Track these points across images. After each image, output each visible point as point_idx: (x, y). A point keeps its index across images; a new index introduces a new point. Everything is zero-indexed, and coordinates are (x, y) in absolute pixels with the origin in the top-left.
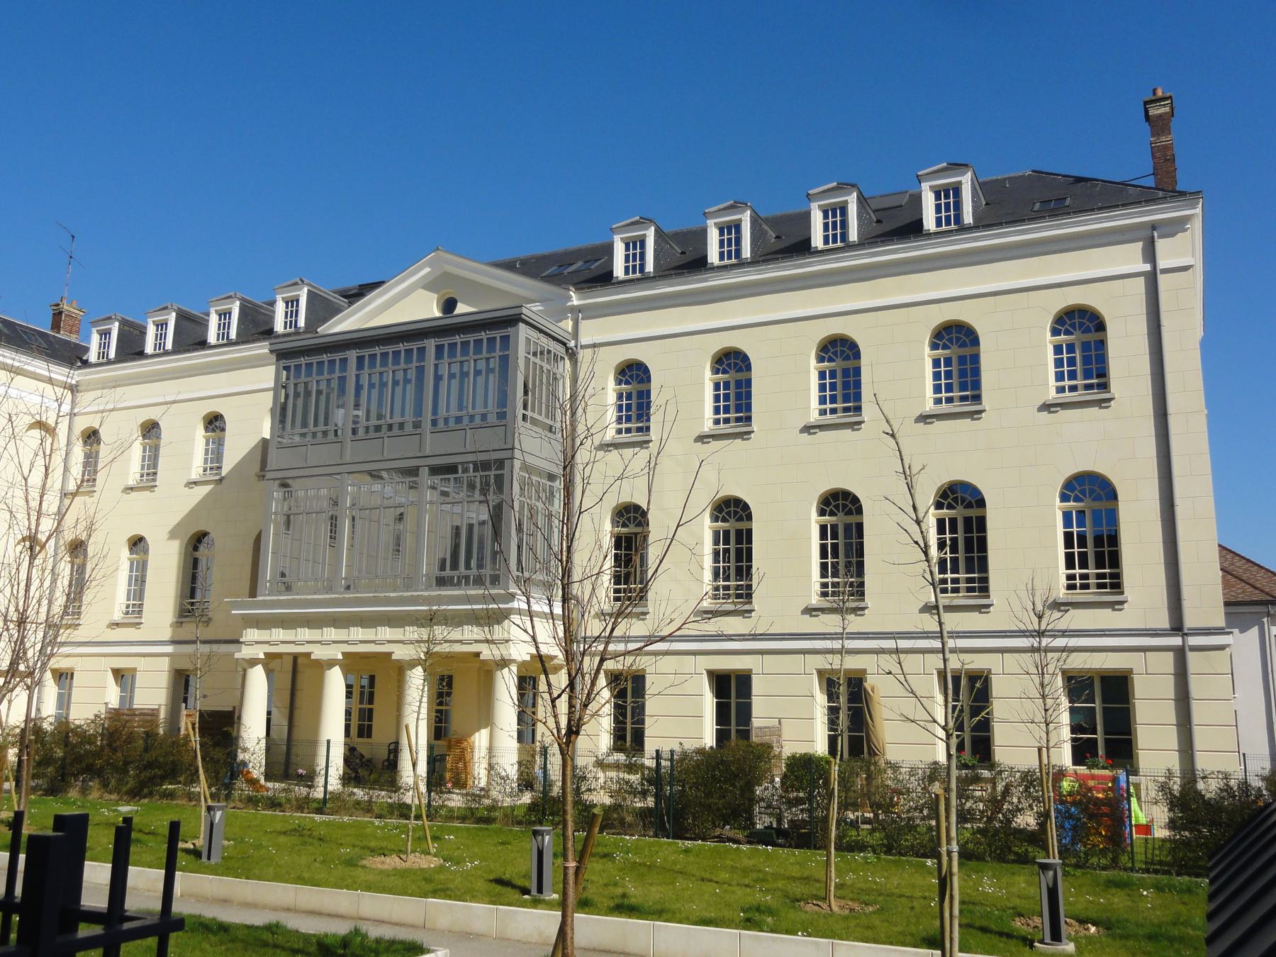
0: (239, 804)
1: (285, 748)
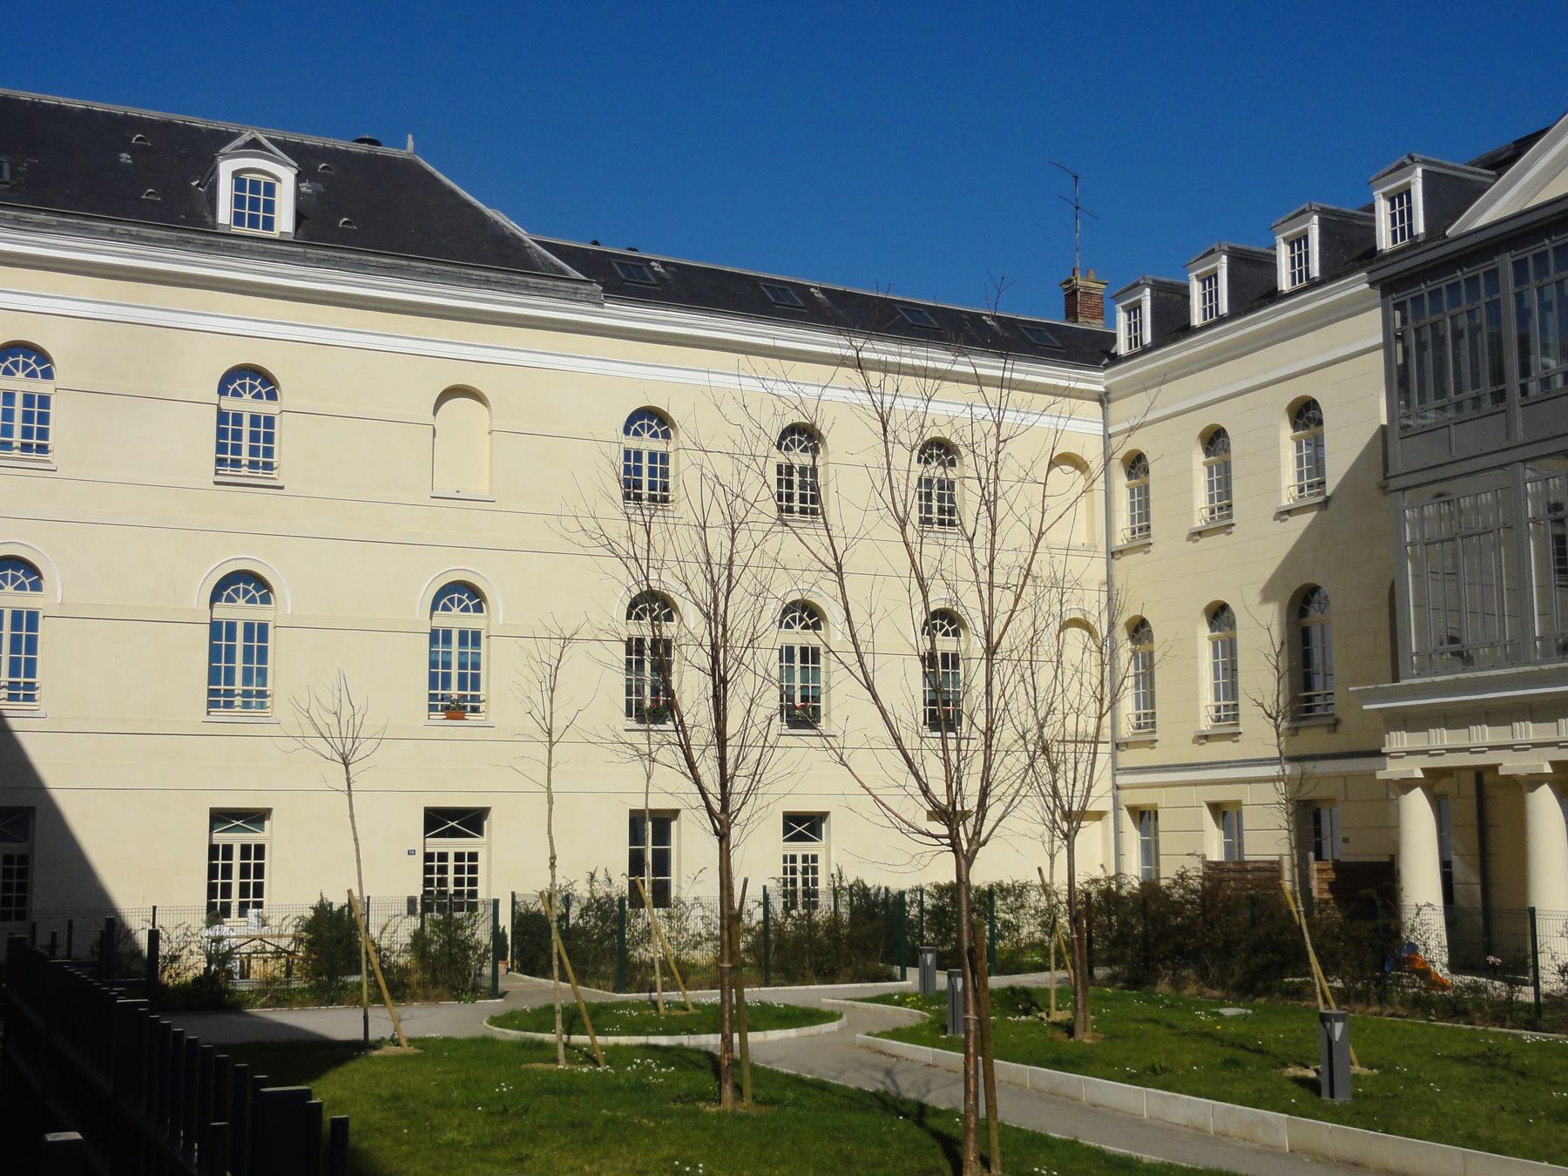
0: (1400, 1010)
1: (1480, 920)
